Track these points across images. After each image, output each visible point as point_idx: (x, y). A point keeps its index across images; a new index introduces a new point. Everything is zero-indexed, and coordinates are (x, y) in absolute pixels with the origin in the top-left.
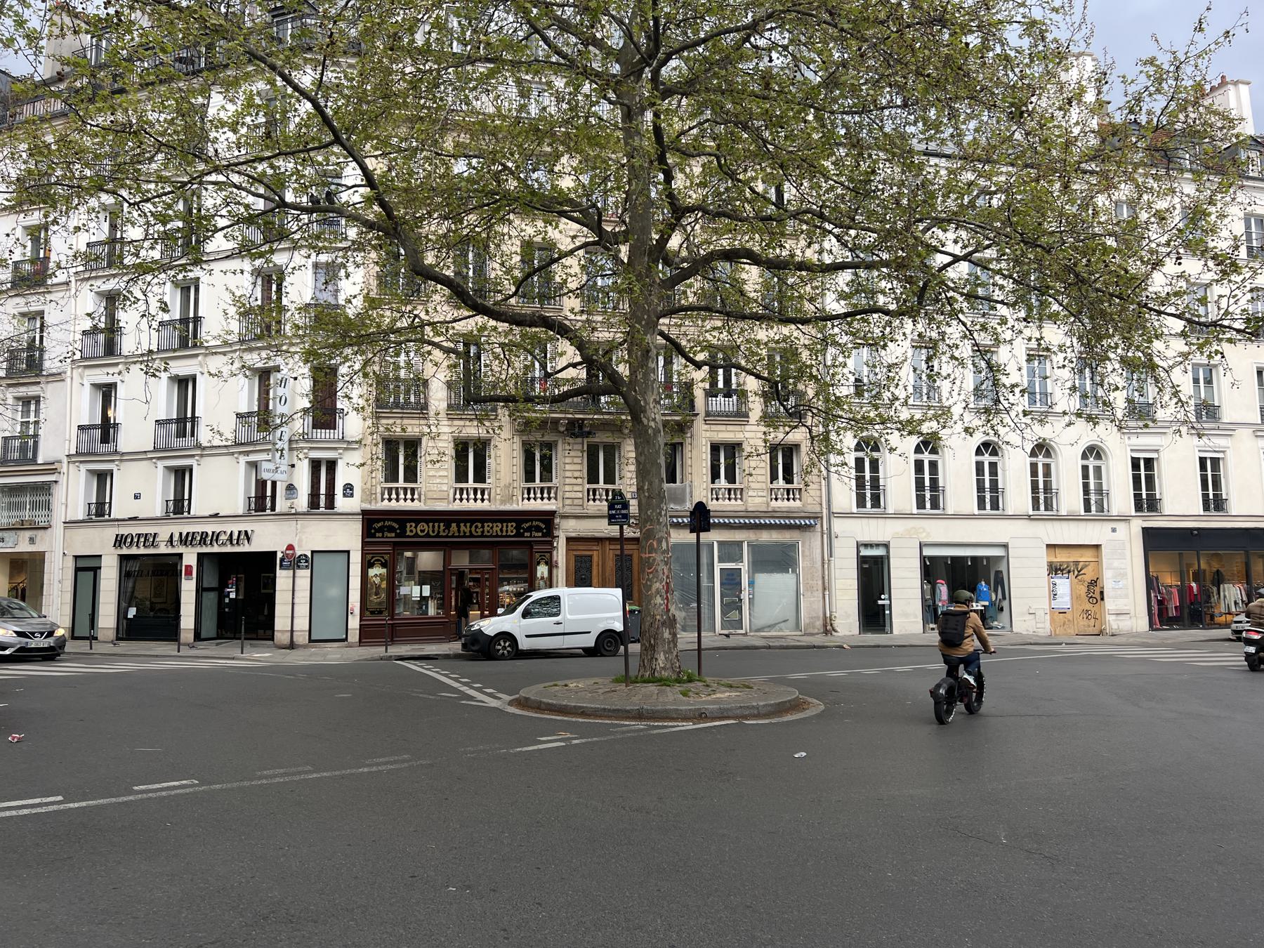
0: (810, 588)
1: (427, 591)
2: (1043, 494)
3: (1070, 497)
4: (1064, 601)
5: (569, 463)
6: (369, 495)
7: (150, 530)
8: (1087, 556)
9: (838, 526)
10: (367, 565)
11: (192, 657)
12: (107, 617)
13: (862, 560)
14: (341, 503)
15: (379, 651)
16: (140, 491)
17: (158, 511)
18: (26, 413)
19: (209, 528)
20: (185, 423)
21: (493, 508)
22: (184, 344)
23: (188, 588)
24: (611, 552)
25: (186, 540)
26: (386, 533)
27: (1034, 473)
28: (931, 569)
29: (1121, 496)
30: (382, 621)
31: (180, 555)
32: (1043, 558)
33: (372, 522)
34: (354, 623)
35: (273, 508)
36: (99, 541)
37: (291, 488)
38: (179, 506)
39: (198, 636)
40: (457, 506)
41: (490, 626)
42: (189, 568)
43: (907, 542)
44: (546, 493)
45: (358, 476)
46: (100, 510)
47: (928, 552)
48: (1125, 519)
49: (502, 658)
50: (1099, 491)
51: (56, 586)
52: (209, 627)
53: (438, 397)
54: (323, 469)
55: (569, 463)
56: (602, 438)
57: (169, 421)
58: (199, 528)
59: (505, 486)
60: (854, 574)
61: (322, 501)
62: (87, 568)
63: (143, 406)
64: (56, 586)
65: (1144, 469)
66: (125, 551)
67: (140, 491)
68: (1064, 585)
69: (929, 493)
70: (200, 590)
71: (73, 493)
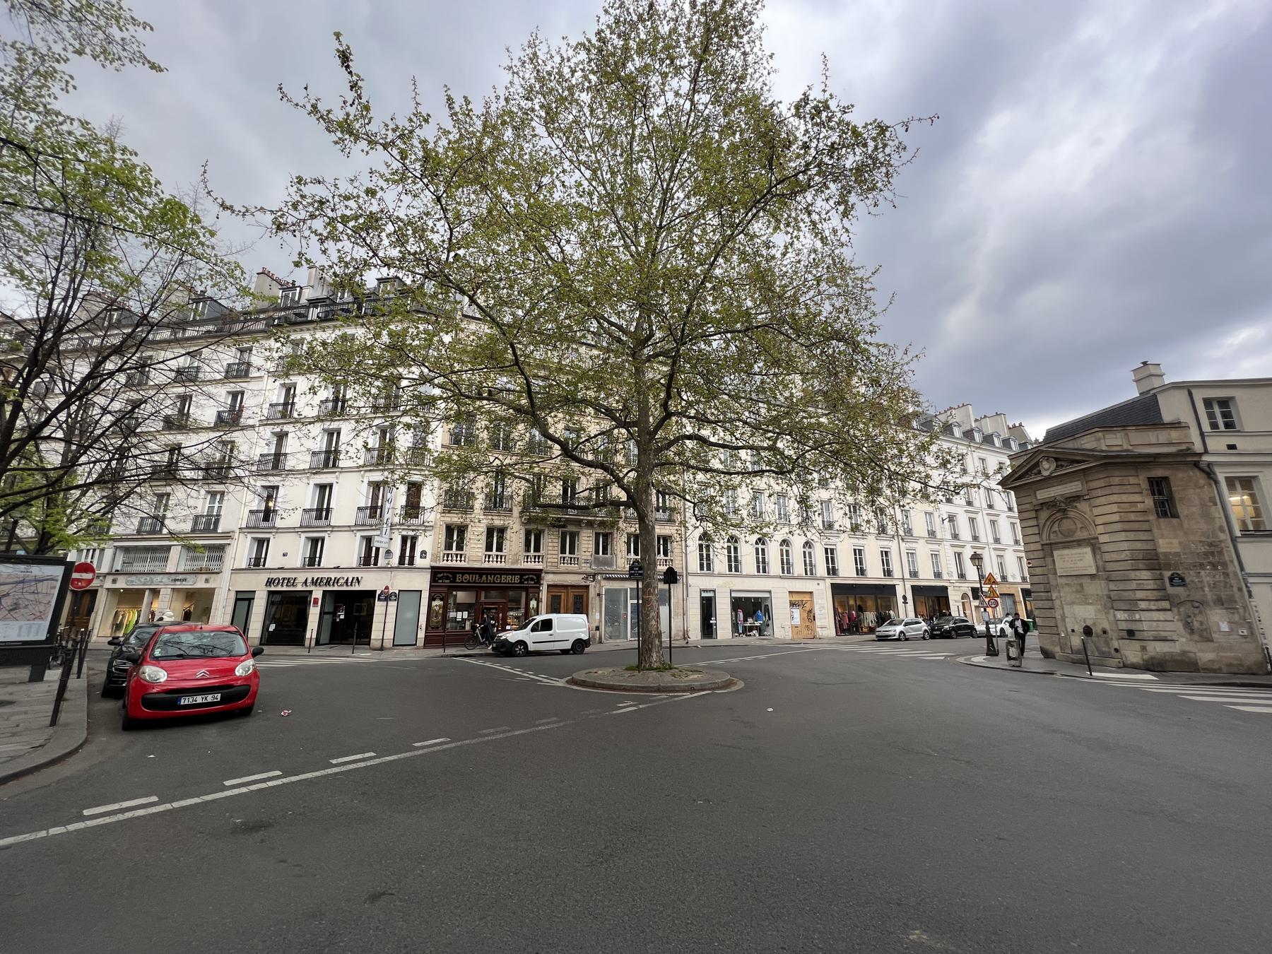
0: (677, 614)
1: (465, 615)
2: (786, 565)
3: (798, 568)
4: (797, 621)
5: (550, 543)
6: (435, 557)
7: (292, 575)
8: (807, 598)
9: (691, 580)
10: (431, 599)
11: (313, 657)
12: (255, 630)
13: (702, 599)
14: (418, 561)
15: (439, 652)
16: (287, 552)
17: (299, 565)
18: (213, 501)
19: (333, 575)
20: (322, 512)
21: (507, 567)
22: (326, 465)
23: (314, 613)
24: (571, 593)
25: (315, 583)
26: (444, 580)
27: (757, 553)
28: (737, 604)
29: (821, 569)
30: (439, 635)
31: (311, 592)
32: (787, 598)
33: (436, 573)
34: (421, 634)
35: (376, 564)
36: (257, 583)
37: (388, 552)
38: (313, 561)
39: (318, 643)
40: (486, 565)
41: (512, 636)
42: (316, 601)
43: (724, 588)
44: (538, 558)
45: (430, 545)
46: (258, 562)
47: (734, 595)
48: (823, 579)
49: (519, 655)
50: (811, 564)
51: (221, 610)
52: (325, 637)
53: (479, 503)
54: (409, 542)
55: (550, 543)
56: (571, 528)
57: (311, 510)
58: (326, 575)
59: (514, 554)
60: (698, 606)
61: (406, 560)
62: (244, 599)
63: (296, 496)
64: (221, 610)
65: (830, 553)
66: (273, 588)
67: (287, 552)
68: (797, 612)
69: (734, 564)
70: (322, 613)
71: (240, 551)
